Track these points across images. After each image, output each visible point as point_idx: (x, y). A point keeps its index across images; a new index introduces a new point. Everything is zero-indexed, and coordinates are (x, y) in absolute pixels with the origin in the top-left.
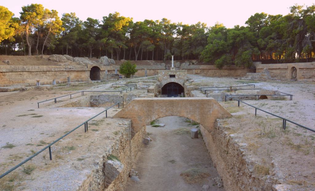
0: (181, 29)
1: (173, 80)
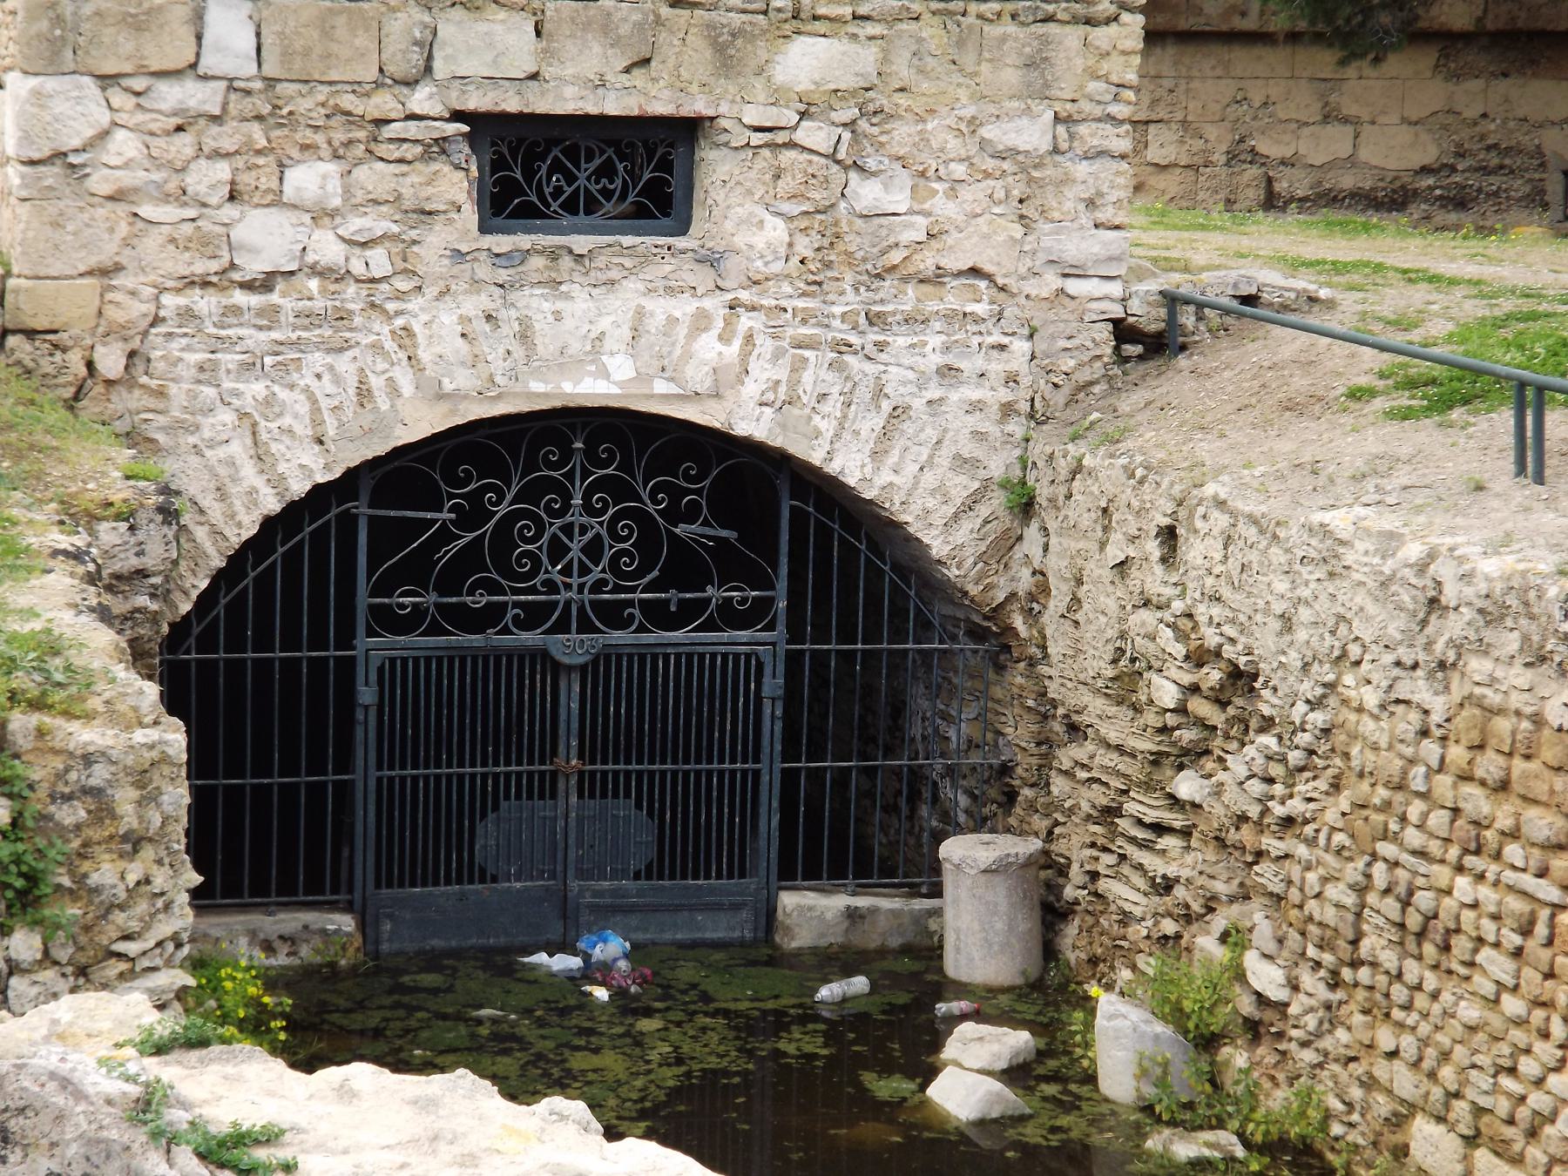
1: (609, 332)
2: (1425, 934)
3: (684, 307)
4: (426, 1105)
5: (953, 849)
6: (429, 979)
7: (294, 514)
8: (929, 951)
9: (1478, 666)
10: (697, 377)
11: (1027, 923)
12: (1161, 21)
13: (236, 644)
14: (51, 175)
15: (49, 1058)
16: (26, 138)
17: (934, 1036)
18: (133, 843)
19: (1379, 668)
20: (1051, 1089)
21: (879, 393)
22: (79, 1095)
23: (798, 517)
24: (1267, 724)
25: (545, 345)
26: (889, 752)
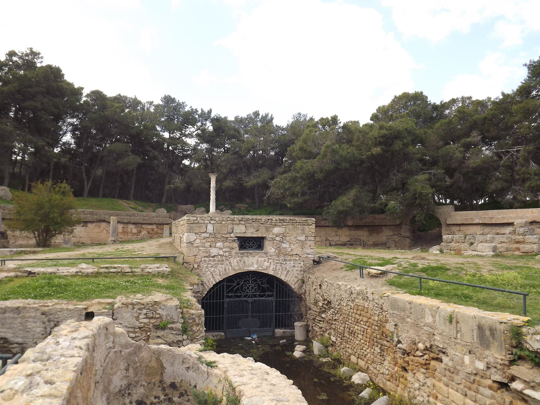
1: (254, 262)
2: (352, 333)
3: (263, 259)
4: (233, 358)
5: (296, 324)
6: (233, 341)
7: (217, 284)
8: (293, 336)
9: (357, 300)
10: (265, 267)
11: (305, 333)
12: (317, 225)
13: (210, 300)
14: (189, 244)
15: (188, 352)
16: (187, 240)
17: (294, 347)
18: (198, 325)
19: (345, 301)
20: (308, 353)
21: (286, 269)
22: (192, 357)
23: (277, 284)
24: (333, 308)
25: (247, 264)
26: (288, 312)
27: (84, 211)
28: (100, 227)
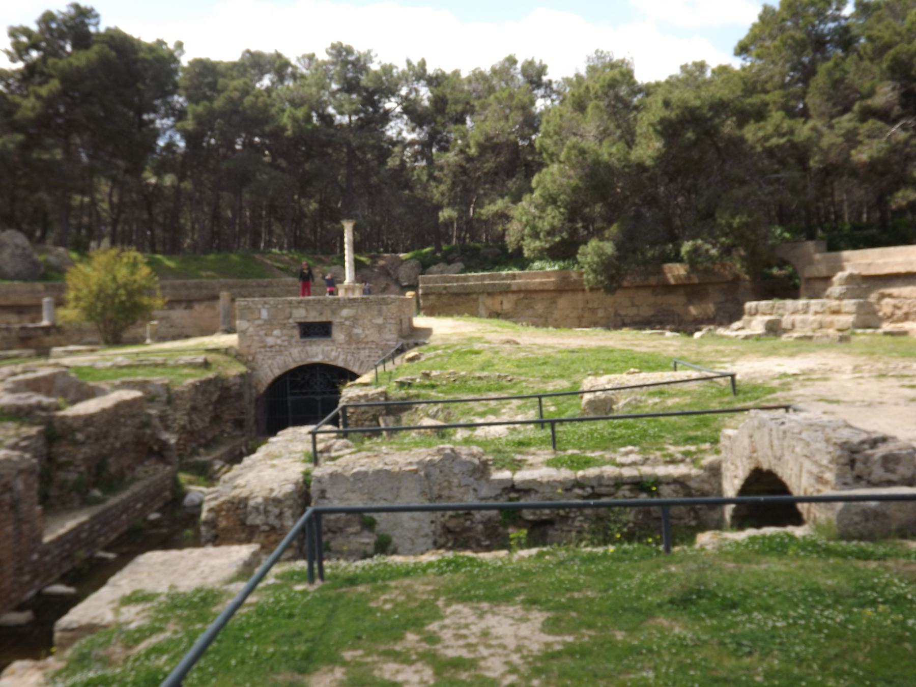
0: (425, 93)
27: (185, 284)
28: (214, 308)
